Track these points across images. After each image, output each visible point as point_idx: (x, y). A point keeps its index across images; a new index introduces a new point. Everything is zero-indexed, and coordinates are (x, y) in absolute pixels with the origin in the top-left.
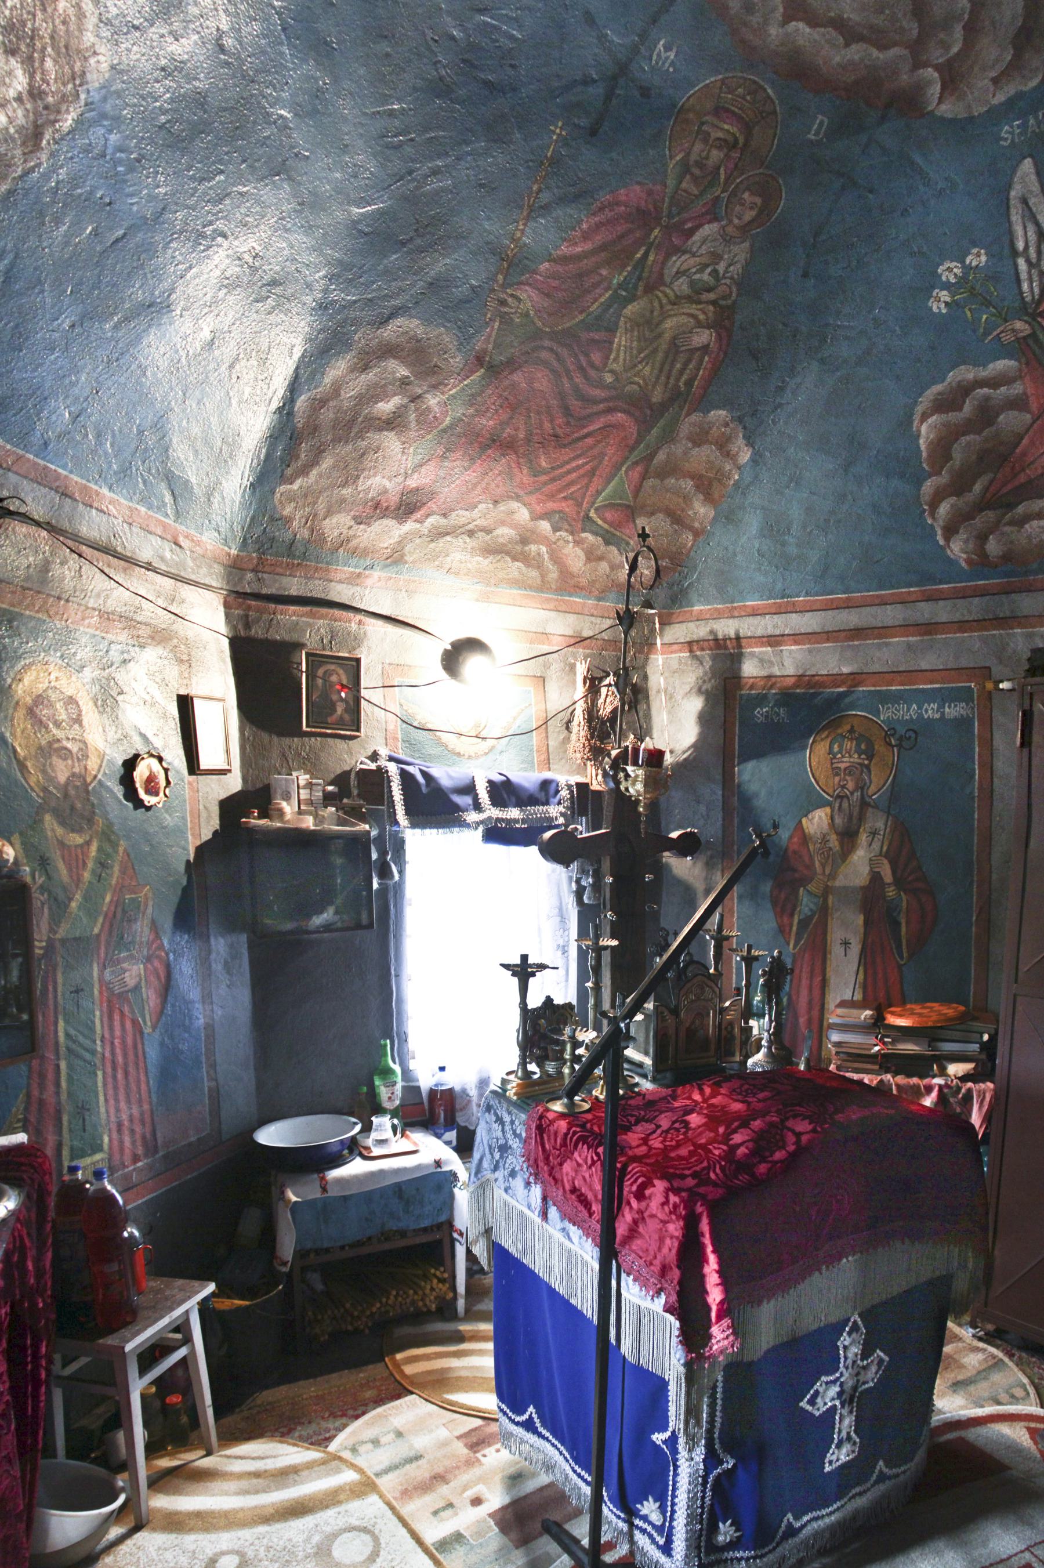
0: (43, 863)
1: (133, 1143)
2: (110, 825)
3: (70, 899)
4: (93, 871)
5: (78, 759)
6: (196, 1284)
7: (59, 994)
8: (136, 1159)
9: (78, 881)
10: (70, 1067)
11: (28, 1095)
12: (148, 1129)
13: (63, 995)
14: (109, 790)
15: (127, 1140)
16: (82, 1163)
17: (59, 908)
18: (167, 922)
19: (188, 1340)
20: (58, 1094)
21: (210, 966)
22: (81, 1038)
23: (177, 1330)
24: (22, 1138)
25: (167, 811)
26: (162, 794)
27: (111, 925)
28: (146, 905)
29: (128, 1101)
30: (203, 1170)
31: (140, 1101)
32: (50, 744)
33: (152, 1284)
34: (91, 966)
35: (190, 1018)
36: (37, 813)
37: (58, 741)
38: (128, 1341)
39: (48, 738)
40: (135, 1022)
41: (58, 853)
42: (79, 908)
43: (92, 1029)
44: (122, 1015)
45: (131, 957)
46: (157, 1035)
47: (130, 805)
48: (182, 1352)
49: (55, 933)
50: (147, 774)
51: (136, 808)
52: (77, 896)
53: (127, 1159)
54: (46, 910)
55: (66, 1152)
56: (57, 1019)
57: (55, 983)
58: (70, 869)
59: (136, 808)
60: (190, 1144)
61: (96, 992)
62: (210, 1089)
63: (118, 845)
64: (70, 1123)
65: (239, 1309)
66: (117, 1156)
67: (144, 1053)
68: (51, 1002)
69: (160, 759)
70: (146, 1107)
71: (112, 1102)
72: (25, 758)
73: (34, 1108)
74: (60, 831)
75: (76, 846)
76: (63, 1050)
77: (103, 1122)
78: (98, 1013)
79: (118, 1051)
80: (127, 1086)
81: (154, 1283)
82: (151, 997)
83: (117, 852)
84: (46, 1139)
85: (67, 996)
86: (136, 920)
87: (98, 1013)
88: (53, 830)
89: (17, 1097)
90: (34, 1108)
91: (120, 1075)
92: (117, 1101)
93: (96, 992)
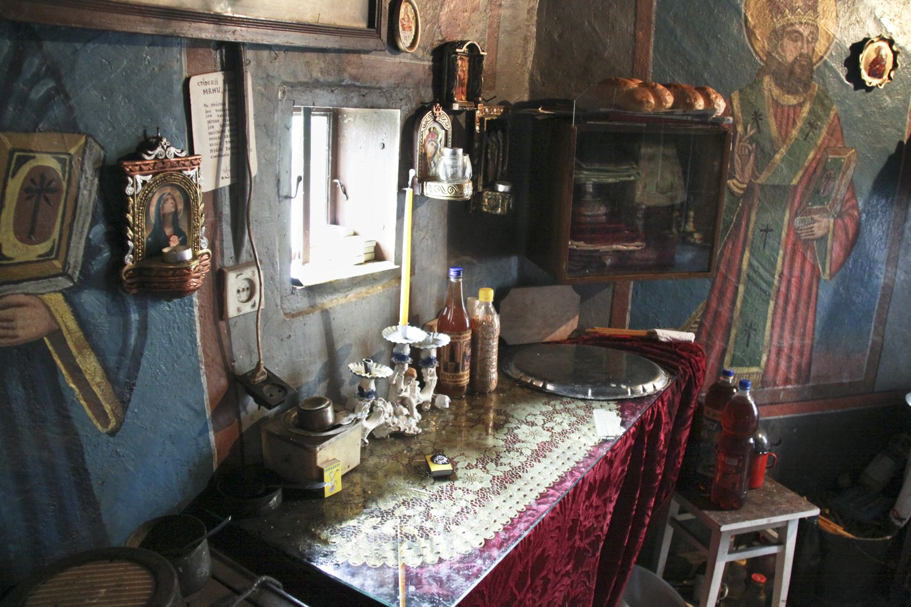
0: (757, 117)
1: (789, 368)
2: (825, 92)
3: (775, 152)
4: (801, 130)
5: (808, 42)
6: (804, 501)
7: (750, 229)
8: (787, 381)
9: (785, 137)
10: (747, 291)
11: (708, 306)
12: (804, 361)
13: (754, 231)
14: (832, 70)
15: (783, 364)
16: (734, 370)
17: (764, 157)
18: (866, 184)
19: (781, 542)
20: (732, 310)
21: (903, 232)
22: (761, 271)
23: (777, 530)
24: (690, 337)
25: (888, 94)
26: (885, 77)
27: (810, 180)
28: (848, 167)
29: (793, 333)
30: (847, 410)
31: (803, 335)
32: (784, 27)
33: (768, 485)
34: (784, 211)
35: (870, 276)
36: (758, 75)
37: (792, 25)
38: (726, 523)
39: (783, 22)
40: (814, 267)
41: (772, 110)
42: (782, 160)
43: (773, 265)
44: (804, 259)
45: (824, 210)
46: (833, 283)
47: (851, 85)
48: (773, 550)
49: (757, 178)
50: (874, 56)
51: (856, 89)
52: (782, 150)
53: (780, 378)
54: (752, 158)
55: (727, 358)
56: (744, 250)
57: (748, 220)
58: (780, 127)
59: (856, 89)
60: (842, 384)
61: (784, 235)
62: (874, 342)
63: (830, 109)
64: (737, 336)
65: (841, 536)
66: (771, 375)
67: (817, 294)
68: (742, 235)
69: (891, 42)
70: (807, 341)
71: (777, 329)
72: (754, 27)
73: (710, 316)
74: (776, 92)
75: (789, 106)
76: (744, 277)
77: (765, 344)
78: (781, 252)
79: (793, 289)
80: (795, 318)
81: (770, 485)
82: (836, 249)
83: (828, 116)
84: (714, 343)
85: (756, 233)
86: (834, 179)
87: (781, 252)
88: (770, 91)
89: (698, 303)
90: (710, 316)
91: (790, 309)
92: (782, 329)
93: (784, 235)
